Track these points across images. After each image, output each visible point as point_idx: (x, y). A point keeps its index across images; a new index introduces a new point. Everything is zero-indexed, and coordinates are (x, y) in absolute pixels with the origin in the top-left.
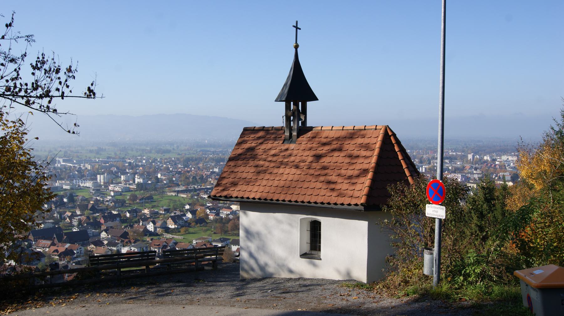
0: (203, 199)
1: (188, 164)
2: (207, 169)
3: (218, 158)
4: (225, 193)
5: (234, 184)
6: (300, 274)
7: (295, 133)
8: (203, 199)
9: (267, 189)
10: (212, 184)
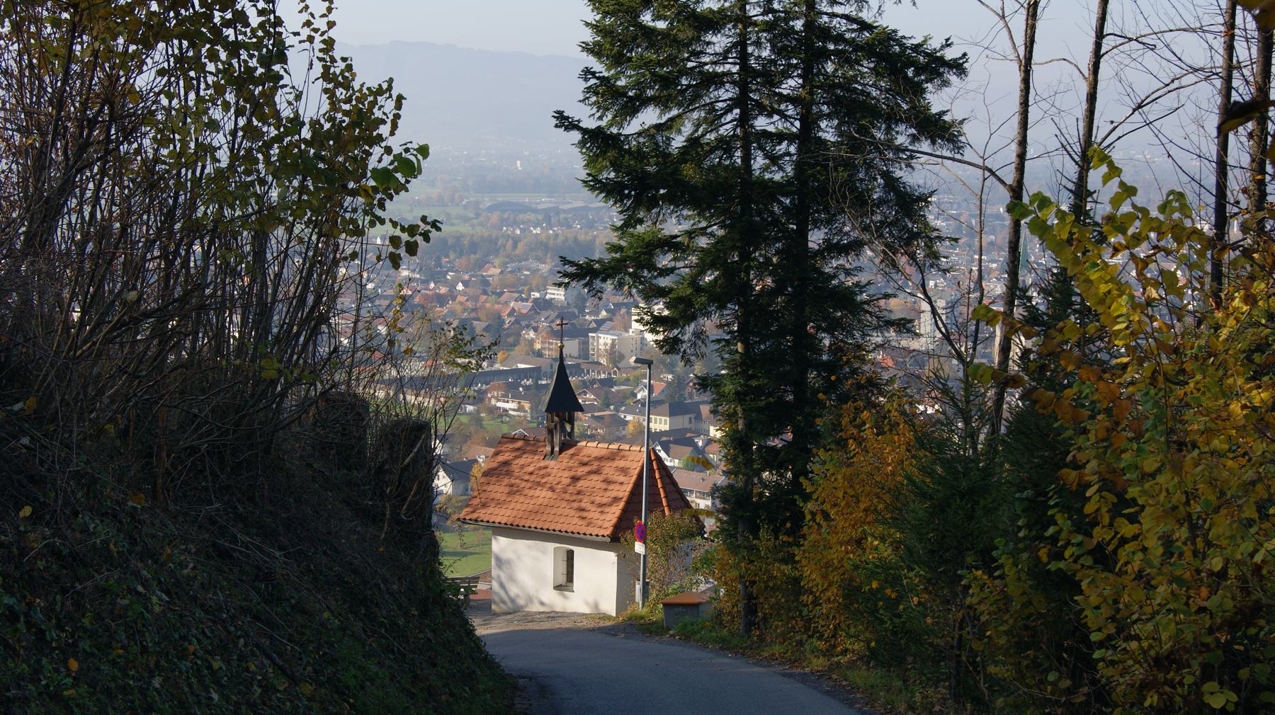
0: (501, 416)
1: (439, 264)
2: (519, 287)
3: (566, 239)
4: (474, 516)
5: (484, 505)
6: (550, 606)
7: (557, 449)
8: (501, 416)
9: (515, 513)
10: (539, 354)
